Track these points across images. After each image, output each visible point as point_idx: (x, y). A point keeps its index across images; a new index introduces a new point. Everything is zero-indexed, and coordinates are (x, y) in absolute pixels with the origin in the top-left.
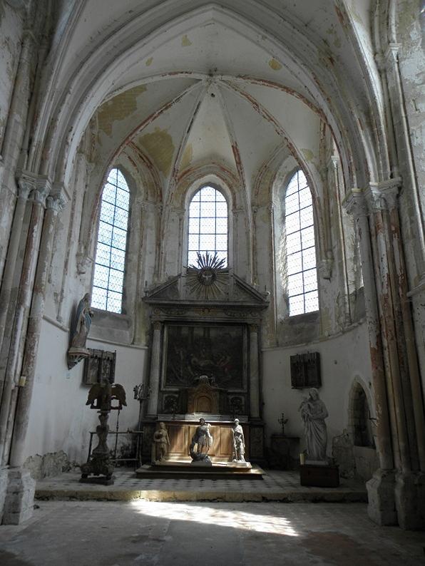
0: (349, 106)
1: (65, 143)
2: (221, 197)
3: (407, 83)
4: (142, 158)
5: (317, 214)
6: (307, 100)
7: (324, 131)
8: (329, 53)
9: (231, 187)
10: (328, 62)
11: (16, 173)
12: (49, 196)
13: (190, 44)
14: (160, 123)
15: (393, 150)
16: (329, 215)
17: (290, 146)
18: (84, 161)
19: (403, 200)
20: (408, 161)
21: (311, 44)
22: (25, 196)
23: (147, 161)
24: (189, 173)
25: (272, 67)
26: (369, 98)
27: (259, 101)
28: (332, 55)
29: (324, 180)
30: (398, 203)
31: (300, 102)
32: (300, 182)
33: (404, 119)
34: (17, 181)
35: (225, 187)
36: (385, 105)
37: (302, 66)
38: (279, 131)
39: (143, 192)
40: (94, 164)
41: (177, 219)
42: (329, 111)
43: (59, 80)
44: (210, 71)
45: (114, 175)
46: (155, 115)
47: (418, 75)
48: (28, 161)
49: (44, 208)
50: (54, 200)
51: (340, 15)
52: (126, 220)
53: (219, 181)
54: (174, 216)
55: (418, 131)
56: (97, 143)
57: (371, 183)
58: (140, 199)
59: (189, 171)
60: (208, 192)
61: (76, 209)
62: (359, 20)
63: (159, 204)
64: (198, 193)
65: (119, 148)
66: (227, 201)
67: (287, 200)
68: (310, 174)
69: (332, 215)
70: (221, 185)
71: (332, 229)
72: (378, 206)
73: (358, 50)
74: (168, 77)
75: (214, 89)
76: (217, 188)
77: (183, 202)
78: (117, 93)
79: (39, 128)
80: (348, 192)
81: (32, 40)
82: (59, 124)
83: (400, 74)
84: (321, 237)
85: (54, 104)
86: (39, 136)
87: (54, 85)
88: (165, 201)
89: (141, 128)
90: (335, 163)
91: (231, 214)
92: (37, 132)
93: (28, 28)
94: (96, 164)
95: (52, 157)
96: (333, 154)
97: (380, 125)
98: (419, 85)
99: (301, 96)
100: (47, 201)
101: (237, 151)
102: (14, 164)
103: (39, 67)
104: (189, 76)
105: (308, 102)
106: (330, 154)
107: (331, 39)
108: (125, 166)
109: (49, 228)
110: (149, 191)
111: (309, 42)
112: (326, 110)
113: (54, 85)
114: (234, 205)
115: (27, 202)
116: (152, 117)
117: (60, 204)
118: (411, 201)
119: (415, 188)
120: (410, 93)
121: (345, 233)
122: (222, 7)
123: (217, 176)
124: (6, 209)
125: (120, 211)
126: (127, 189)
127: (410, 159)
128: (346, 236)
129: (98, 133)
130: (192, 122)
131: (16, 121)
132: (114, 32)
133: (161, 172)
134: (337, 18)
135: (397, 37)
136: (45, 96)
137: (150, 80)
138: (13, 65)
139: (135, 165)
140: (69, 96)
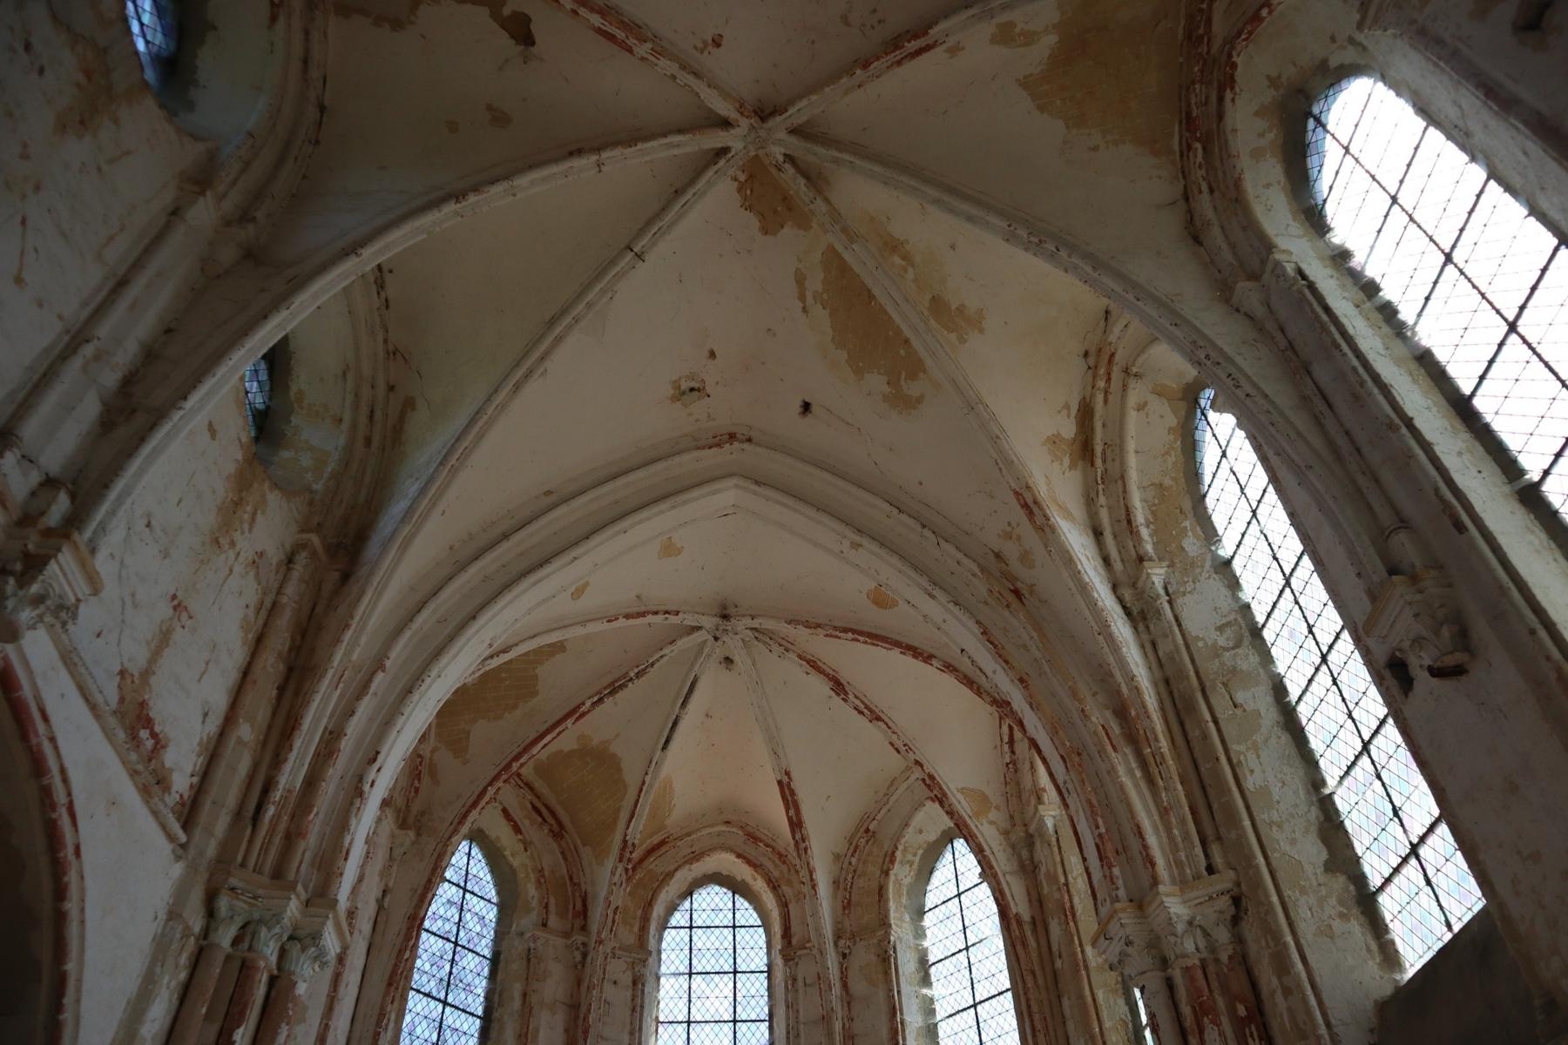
0: (1074, 694)
1: (356, 791)
2: (747, 914)
3: (1201, 644)
4: (540, 814)
5: (1018, 960)
6: (966, 677)
7: (1011, 741)
8: (1009, 577)
9: (774, 886)
10: (1011, 598)
11: (211, 875)
12: (291, 938)
13: (680, 551)
14: (600, 725)
15: (1198, 794)
16: (1053, 963)
17: (930, 782)
18: (389, 825)
19: (1250, 930)
20: (1242, 828)
21: (965, 561)
22: (225, 937)
23: (553, 822)
24: (663, 849)
25: (876, 603)
26: (1120, 679)
27: (844, 676)
28: (1019, 585)
29: (1029, 869)
30: (1239, 940)
31: (948, 680)
32: (960, 868)
33: (1211, 725)
34: (211, 898)
35: (759, 885)
36: (1158, 694)
37: (951, 606)
38: (899, 744)
39: (535, 903)
40: (411, 834)
41: (627, 979)
42: (1027, 708)
43: (363, 640)
44: (724, 607)
45: (467, 863)
46: (583, 709)
47: (1220, 629)
48: (251, 842)
49: (270, 971)
50: (303, 950)
51: (1025, 506)
52: (481, 986)
53: (743, 872)
54: (618, 969)
55: (1251, 756)
56: (426, 779)
57: (1161, 888)
58: (526, 922)
59: (663, 843)
60: (712, 902)
61: (348, 963)
62: (1068, 516)
63: (579, 938)
64: (687, 904)
65: (484, 791)
66: (766, 925)
67: (929, 920)
68: (988, 853)
69: (1058, 963)
70: (749, 879)
71: (1066, 1002)
72: (1189, 946)
73: (1076, 575)
74: (622, 622)
75: (733, 646)
76: (737, 888)
77: (644, 929)
78: (495, 662)
79: (292, 756)
80: (1104, 911)
81: (314, 554)
82: (346, 745)
83: (1179, 625)
84: (1039, 1026)
85: (342, 696)
86: (291, 776)
87: (349, 652)
88: (594, 928)
89: (545, 741)
90: (1050, 823)
91: (779, 961)
92: (287, 767)
93: (310, 531)
94: (418, 834)
95: (316, 829)
96: (1040, 800)
97: (1156, 739)
98: (1228, 650)
99: (949, 668)
100: (283, 953)
101: (793, 793)
102: (211, 850)
103: (319, 610)
104: (673, 619)
105: (969, 682)
106: (1033, 801)
107: (1011, 551)
108: (492, 833)
109: (275, 1034)
110: (552, 901)
111: (960, 556)
112: (1019, 703)
113: (349, 652)
114: (787, 934)
115: (228, 958)
116: (575, 713)
117: (315, 959)
118: (1272, 933)
119: (1275, 899)
120: (1210, 668)
121: (1104, 1014)
122: (757, 483)
123: (739, 856)
124: (165, 981)
125: (469, 962)
126: (492, 894)
127: (1247, 823)
128: (1107, 1024)
129: (433, 752)
130: (675, 724)
131: (240, 741)
132: (506, 536)
133: (588, 849)
134: (1021, 514)
135: (1155, 549)
136: (322, 676)
137: (579, 631)
138: (258, 610)
139: (517, 829)
140: (380, 676)
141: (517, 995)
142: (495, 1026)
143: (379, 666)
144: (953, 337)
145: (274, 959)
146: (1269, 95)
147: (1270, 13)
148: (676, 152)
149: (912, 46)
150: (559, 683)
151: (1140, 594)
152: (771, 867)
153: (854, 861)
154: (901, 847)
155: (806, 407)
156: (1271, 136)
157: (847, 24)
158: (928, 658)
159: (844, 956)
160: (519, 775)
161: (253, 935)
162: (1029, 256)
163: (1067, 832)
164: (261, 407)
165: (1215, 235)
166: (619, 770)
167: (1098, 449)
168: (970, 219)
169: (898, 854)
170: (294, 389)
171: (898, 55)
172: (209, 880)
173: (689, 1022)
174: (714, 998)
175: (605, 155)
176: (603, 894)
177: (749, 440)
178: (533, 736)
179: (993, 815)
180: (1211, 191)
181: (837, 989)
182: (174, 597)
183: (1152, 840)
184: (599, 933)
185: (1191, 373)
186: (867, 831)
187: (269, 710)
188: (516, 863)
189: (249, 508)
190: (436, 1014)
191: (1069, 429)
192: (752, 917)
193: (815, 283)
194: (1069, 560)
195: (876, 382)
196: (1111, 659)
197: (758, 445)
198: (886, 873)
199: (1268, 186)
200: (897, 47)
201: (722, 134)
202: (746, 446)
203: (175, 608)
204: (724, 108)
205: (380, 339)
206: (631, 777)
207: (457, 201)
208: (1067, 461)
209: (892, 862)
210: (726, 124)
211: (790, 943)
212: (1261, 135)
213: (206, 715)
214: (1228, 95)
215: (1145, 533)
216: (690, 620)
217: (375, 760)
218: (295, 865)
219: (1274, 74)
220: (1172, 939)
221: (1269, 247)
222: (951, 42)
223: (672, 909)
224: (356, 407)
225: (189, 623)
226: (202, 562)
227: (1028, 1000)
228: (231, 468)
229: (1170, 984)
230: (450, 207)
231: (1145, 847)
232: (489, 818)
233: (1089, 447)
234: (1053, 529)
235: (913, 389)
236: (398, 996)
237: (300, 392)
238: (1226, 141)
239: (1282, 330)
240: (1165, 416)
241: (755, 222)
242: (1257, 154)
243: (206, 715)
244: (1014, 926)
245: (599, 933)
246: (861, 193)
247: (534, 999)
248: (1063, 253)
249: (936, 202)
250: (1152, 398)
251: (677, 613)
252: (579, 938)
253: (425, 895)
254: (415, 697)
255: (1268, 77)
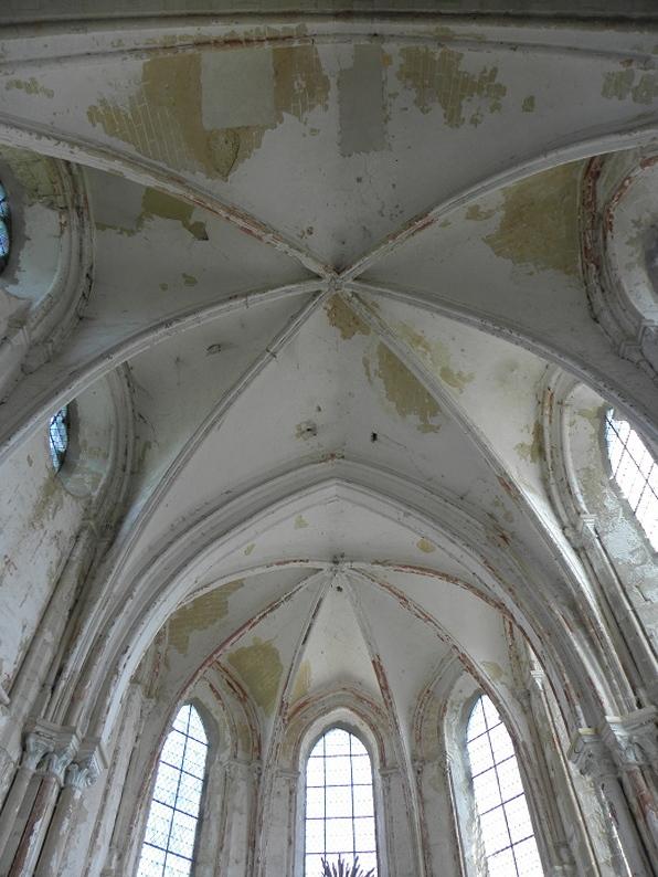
0: (543, 597)
1: (113, 671)
2: (358, 747)
4: (232, 687)
7: (511, 632)
8: (497, 528)
9: (374, 729)
11: (25, 725)
12: (73, 763)
15: (627, 658)
16: (549, 774)
17: (463, 659)
18: (139, 696)
27: (408, 594)
31: (469, 594)
35: (365, 728)
37: (465, 547)
39: (229, 743)
40: (153, 700)
41: (285, 790)
43: (120, 581)
47: (631, 553)
50: (80, 769)
51: (504, 485)
53: (355, 720)
56: (162, 666)
58: (225, 756)
59: (305, 703)
60: (337, 740)
62: (532, 490)
66: (370, 754)
68: (502, 703)
69: (552, 774)
71: (559, 801)
74: (275, 567)
76: (352, 730)
77: (296, 758)
78: (201, 593)
81: (92, 532)
82: (109, 643)
83: (606, 552)
84: (543, 817)
87: (111, 588)
90: (538, 682)
91: (379, 777)
92: (73, 657)
95: (90, 694)
97: (597, 622)
98: (638, 565)
99: (469, 586)
100: (67, 772)
102: (26, 710)
105: (481, 594)
106: (528, 668)
107: (499, 512)
110: (240, 741)
111: (468, 517)
113: (111, 588)
114: (383, 760)
115: (34, 775)
116: (250, 623)
120: (628, 579)
121: (584, 808)
123: (352, 710)
125: (187, 780)
126: (204, 739)
128: (587, 815)
131: (45, 642)
132: (204, 517)
138: (58, 565)
139: (219, 697)
140: (130, 601)
141: (219, 803)
142: (205, 823)
143: (129, 594)
144: (456, 390)
145: (62, 777)
146: (634, 233)
147: (630, 182)
148: (290, 294)
149: (419, 224)
150: (239, 605)
151: (579, 535)
152: (372, 716)
153: (421, 711)
154: (449, 702)
155: (374, 436)
156: (637, 255)
157: (383, 215)
158: (455, 581)
159: (419, 772)
160: (219, 663)
161: (50, 760)
162: (494, 337)
163: (548, 687)
164: (62, 450)
165: (606, 316)
166: (278, 658)
167: (548, 450)
168: (459, 319)
169: (448, 706)
170: (81, 439)
171: (412, 229)
172: (24, 728)
173: (353, 818)
174: (339, 803)
175: (249, 298)
176: (270, 736)
177: (343, 457)
178: (226, 638)
179: (503, 678)
180: (603, 291)
181: (414, 795)
182: (6, 557)
183: (599, 687)
184: (268, 761)
185: (601, 401)
186: (428, 692)
187: (64, 624)
188: (218, 718)
189: (52, 506)
190: (169, 817)
191: (529, 440)
192: (363, 750)
193: (374, 365)
194: (533, 517)
195: (413, 419)
196: (564, 575)
197: (348, 460)
198: (442, 719)
199: (637, 284)
200: (411, 225)
201: (315, 282)
202: (341, 460)
203: (6, 563)
204: (316, 268)
205: (130, 409)
206: (286, 664)
207: (167, 326)
208: (529, 457)
209: (445, 711)
210: (318, 277)
211: (385, 765)
212: (632, 255)
213: (24, 627)
214: (609, 233)
215: (580, 498)
216: (317, 565)
217: (126, 651)
218: (77, 716)
219: (636, 218)
220: (618, 752)
221: (640, 318)
222: (442, 219)
223: (313, 745)
224: (117, 448)
225: (15, 572)
226: (24, 537)
227: (534, 799)
228: (41, 482)
229: (620, 782)
230: (163, 330)
231: (595, 691)
232: (200, 689)
233: (543, 450)
234: (523, 499)
235: (434, 421)
236: (144, 805)
237: (85, 441)
238: (610, 261)
239: (651, 366)
240: (587, 428)
241: (339, 332)
242: (629, 267)
243: (24, 627)
244: (522, 749)
245: (268, 761)
246: (398, 311)
247: (229, 805)
248: (514, 334)
249: (438, 312)
250: (577, 417)
251: (307, 561)
252: (256, 765)
253: (159, 740)
254: (152, 612)
255: (633, 221)
